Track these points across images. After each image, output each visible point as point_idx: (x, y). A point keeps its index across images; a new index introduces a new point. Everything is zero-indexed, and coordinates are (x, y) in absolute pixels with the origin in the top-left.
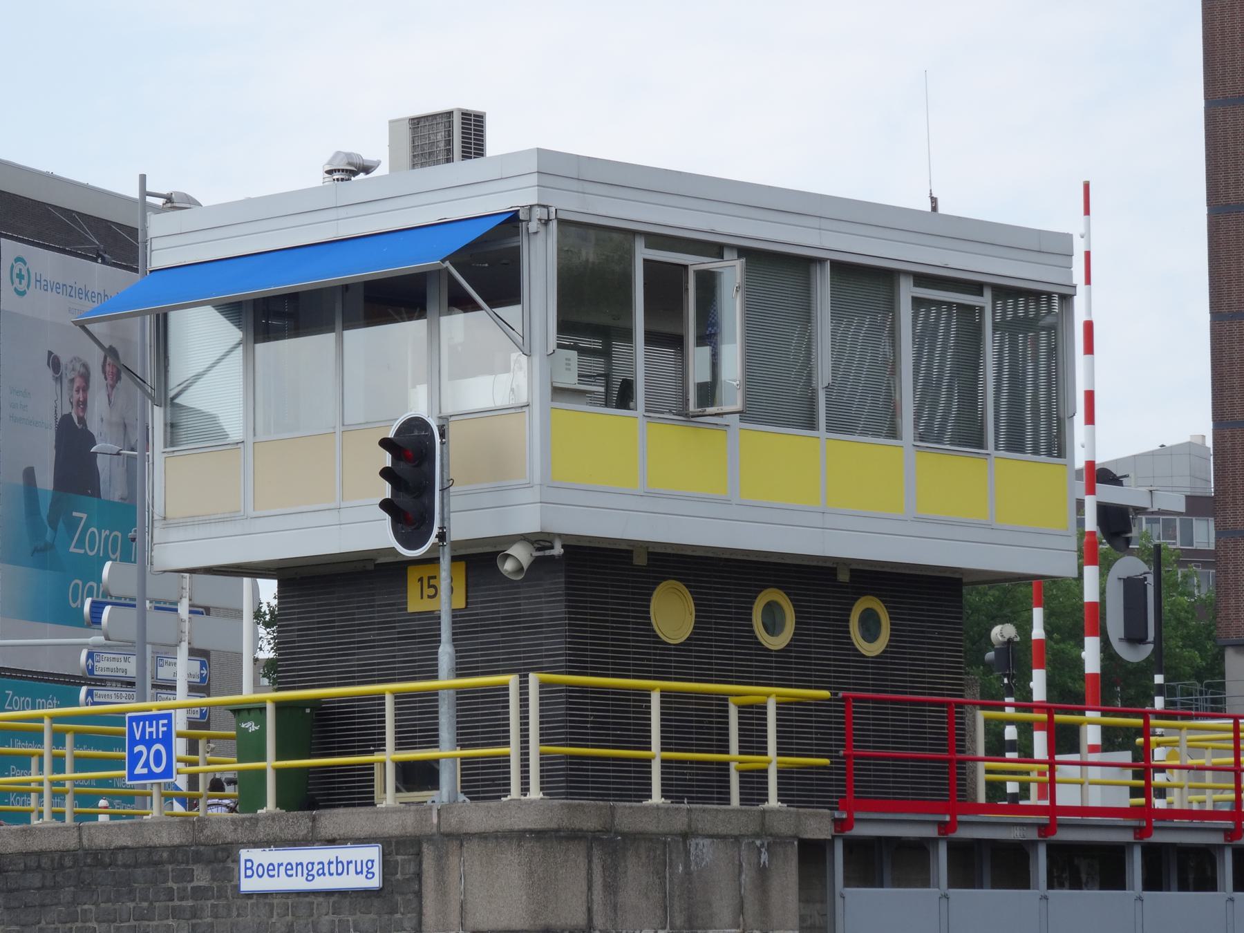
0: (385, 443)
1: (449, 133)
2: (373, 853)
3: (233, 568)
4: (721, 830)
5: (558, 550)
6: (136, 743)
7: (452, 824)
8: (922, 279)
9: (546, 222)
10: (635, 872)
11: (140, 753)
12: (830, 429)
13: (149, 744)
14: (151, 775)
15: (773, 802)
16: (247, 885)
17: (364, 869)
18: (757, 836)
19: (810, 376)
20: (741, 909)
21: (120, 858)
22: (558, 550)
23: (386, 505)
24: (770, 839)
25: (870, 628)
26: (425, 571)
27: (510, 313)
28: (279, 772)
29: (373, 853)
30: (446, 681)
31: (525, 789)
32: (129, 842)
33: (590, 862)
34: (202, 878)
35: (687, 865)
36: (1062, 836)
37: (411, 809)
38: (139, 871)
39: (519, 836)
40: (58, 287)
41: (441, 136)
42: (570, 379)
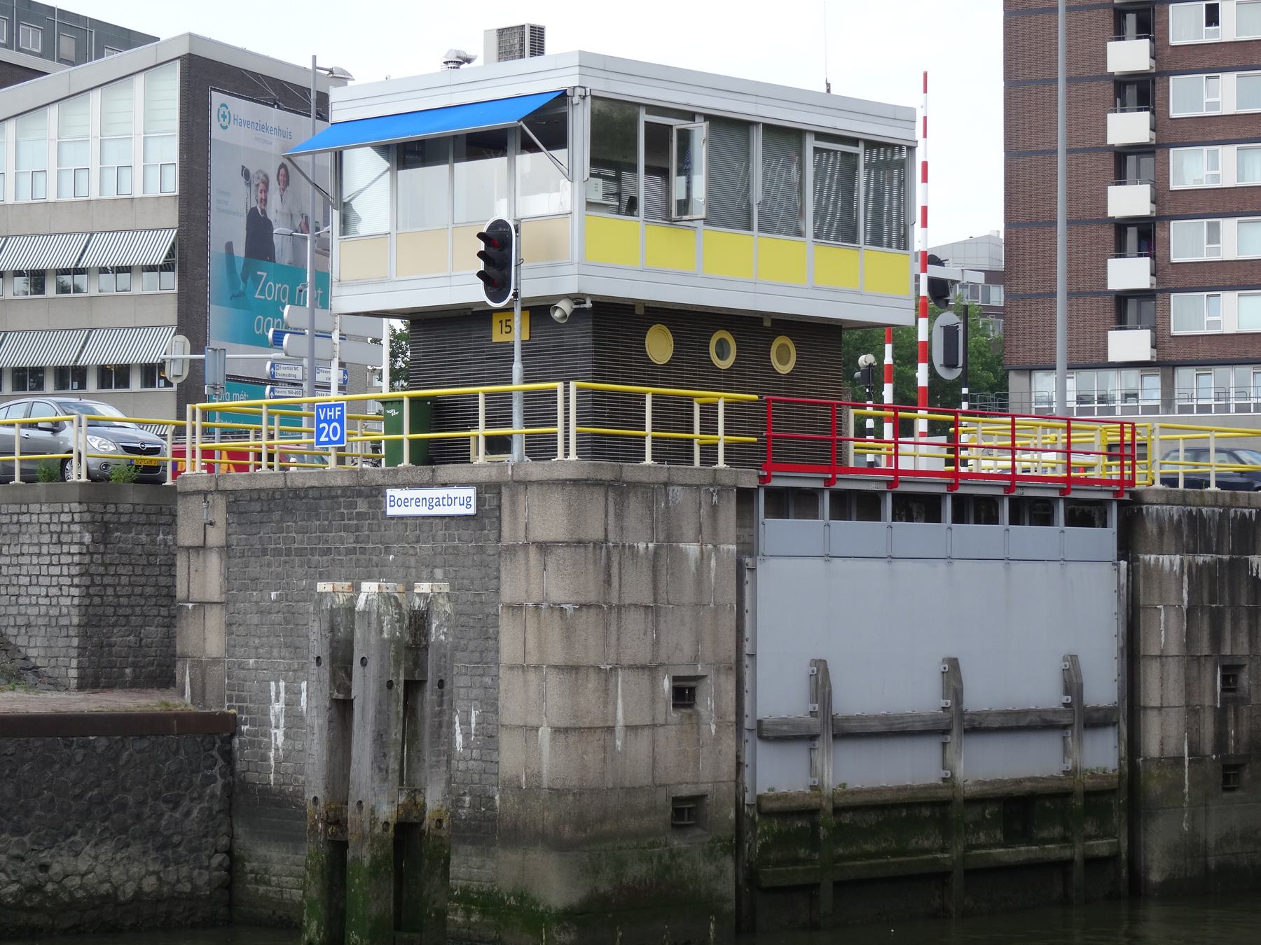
0: (481, 236)
1: (522, 39)
2: (471, 492)
4: (689, 481)
5: (589, 305)
7: (521, 474)
8: (820, 136)
9: (584, 97)
10: (635, 506)
11: (324, 428)
13: (329, 422)
14: (331, 442)
15: (721, 464)
16: (391, 511)
18: (711, 485)
19: (748, 190)
22: (589, 305)
23: (481, 275)
24: (719, 487)
27: (560, 154)
28: (412, 441)
29: (471, 492)
30: (517, 385)
31: (567, 454)
33: (607, 500)
34: (362, 506)
35: (667, 503)
36: (902, 488)
39: (562, 483)
40: (248, 124)
41: (517, 41)
42: (598, 197)
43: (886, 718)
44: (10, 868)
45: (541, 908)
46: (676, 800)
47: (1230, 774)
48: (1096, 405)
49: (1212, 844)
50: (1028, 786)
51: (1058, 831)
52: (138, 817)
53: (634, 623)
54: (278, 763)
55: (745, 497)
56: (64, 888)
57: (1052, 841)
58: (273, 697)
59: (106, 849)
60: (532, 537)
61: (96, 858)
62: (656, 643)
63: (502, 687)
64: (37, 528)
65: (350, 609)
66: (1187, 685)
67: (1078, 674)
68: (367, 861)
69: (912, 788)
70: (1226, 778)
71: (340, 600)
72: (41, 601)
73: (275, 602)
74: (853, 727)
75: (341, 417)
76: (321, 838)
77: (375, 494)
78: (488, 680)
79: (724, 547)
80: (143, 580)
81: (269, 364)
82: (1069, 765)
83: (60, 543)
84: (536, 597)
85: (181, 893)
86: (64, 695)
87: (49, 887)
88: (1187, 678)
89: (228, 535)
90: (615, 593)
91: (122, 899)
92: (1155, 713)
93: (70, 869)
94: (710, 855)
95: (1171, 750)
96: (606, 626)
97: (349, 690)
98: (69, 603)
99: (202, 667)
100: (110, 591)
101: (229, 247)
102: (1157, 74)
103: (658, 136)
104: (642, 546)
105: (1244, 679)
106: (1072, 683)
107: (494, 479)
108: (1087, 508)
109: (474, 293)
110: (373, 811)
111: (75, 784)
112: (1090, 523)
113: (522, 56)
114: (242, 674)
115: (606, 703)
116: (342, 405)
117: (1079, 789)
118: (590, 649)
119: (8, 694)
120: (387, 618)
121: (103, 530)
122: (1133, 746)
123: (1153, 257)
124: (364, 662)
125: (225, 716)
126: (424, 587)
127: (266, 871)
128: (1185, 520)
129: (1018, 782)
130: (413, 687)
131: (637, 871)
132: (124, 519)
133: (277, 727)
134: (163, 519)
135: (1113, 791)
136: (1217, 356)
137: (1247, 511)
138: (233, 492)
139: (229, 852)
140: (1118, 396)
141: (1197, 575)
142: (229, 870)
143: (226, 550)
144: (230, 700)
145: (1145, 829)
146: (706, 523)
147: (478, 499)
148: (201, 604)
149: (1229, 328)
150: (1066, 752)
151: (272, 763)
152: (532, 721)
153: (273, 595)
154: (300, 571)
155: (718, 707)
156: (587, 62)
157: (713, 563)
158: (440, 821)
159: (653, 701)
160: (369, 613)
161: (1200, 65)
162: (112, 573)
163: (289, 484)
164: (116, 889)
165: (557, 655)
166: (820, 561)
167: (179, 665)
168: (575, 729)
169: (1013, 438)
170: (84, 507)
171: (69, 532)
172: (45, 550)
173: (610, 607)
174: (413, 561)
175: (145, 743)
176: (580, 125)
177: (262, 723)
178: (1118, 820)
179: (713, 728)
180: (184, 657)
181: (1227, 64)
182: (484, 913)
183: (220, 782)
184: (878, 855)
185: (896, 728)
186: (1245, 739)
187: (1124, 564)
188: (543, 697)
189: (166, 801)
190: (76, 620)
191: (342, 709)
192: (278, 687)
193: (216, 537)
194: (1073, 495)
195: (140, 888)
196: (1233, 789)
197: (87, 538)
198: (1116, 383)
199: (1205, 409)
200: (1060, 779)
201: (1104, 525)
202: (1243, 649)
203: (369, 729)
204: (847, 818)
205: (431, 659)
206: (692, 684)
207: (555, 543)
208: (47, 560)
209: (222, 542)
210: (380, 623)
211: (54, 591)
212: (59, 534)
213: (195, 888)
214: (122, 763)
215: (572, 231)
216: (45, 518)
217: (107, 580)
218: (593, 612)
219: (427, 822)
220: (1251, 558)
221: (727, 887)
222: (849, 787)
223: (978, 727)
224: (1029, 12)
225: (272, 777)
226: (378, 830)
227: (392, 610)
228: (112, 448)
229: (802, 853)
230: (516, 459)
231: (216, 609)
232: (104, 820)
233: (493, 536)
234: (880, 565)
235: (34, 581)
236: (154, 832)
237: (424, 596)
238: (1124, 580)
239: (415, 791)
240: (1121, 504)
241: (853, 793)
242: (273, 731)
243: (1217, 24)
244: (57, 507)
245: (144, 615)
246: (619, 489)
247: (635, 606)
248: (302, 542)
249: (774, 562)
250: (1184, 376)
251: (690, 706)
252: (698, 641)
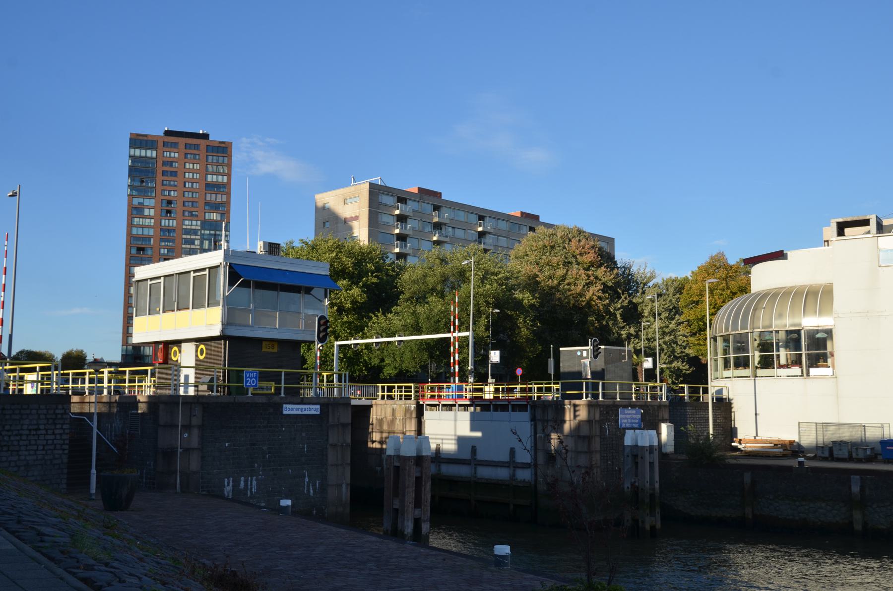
2: (318, 406)
3: (776, 456)
6: (248, 378)
11: (248, 380)
16: (285, 412)
29: (318, 406)
37: (9, 427)
58: (226, 484)
73: (227, 447)
77: (279, 407)
116: (257, 372)
153: (227, 445)
163: (236, 401)
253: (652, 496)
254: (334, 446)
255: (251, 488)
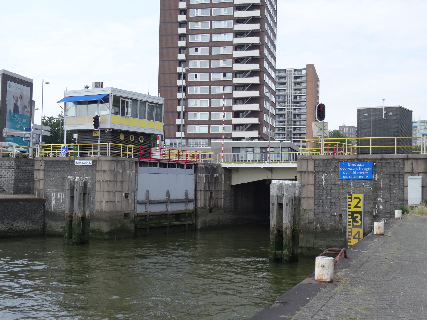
0: (94, 118)
1: (99, 84)
2: (91, 161)
4: (128, 160)
5: (112, 130)
7: (100, 159)
8: (149, 102)
9: (112, 95)
10: (119, 164)
12: (139, 118)
13: (64, 149)
14: (64, 152)
15: (133, 157)
16: (76, 164)
17: (90, 163)
19: (137, 112)
20: (129, 169)
21: (61, 161)
22: (112, 130)
23: (93, 125)
25: (141, 139)
26: (98, 131)
27: (107, 104)
28: (80, 152)
29: (91, 161)
30: (99, 143)
31: (108, 155)
32: (62, 159)
34: (70, 163)
36: (161, 162)
38: (63, 162)
39: (108, 160)
40: (14, 87)
41: (98, 84)
42: (113, 112)
43: (158, 200)
44: (6, 225)
45: (102, 232)
46: (125, 213)
47: (211, 210)
48: (174, 145)
49: (208, 221)
50: (179, 212)
51: (184, 219)
52: (28, 216)
53: (119, 184)
54: (53, 207)
55: (136, 163)
56: (15, 229)
57: (183, 221)
59: (23, 222)
60: (102, 169)
61: (21, 224)
62: (122, 187)
63: (96, 194)
64: (5, 166)
65: (74, 181)
66: (204, 195)
67: (188, 193)
68: (77, 223)
69: (161, 212)
70: (210, 211)
71: (72, 179)
72: (6, 178)
74: (153, 202)
75: (66, 148)
76: (68, 220)
77: (73, 161)
78: (93, 193)
79: (133, 171)
80: (25, 175)
81: (24, 134)
82: (186, 208)
83: (10, 168)
84: (103, 179)
85: (36, 230)
86: (11, 195)
87: (13, 229)
88: (204, 194)
89: (44, 168)
90: (116, 179)
91: (25, 231)
92: (199, 200)
93: (17, 225)
94: (130, 223)
95: (202, 206)
96: (114, 184)
97: (74, 195)
98: (12, 179)
99: (39, 191)
100: (19, 177)
101: (10, 110)
102: (186, 86)
103: (123, 102)
104: (120, 171)
105: (213, 194)
106: (187, 195)
107: (95, 159)
108: (189, 166)
109: (92, 127)
110: (78, 215)
111: (18, 211)
112: (189, 168)
113: (99, 87)
114: (47, 192)
115: (114, 197)
117: (187, 212)
118: (112, 188)
119: (1, 195)
120: (81, 183)
121: (18, 166)
122: (196, 205)
123: (185, 119)
124: (77, 190)
125: (44, 199)
126: (86, 178)
127: (51, 226)
128: (205, 168)
129: (178, 211)
130: (85, 194)
131: (119, 225)
132: (22, 164)
133: (53, 201)
134: (28, 164)
135: (192, 213)
136: (195, 137)
137: (214, 166)
138: (46, 160)
139: (44, 223)
140: (178, 144)
141: (206, 177)
142: (44, 226)
143: (44, 170)
144: (44, 196)
145: (79, 241)
146: (130, 167)
147: (92, 162)
148: (39, 180)
149: (198, 132)
150: (185, 206)
151: (52, 207)
152: (101, 200)
153: (53, 178)
154: (58, 174)
155: (132, 198)
156: (113, 89)
157: (131, 174)
158: (88, 217)
159: (122, 197)
160: (78, 182)
161: (194, 85)
162: (337, 185)
164: (24, 229)
165: (106, 189)
166: (148, 174)
167: (35, 190)
168: (109, 202)
169: (170, 153)
170: (15, 162)
171: (12, 166)
172: (7, 169)
173: (115, 181)
174: (80, 173)
175: (30, 204)
176: (111, 99)
177: (51, 200)
178: (193, 218)
179: (131, 202)
180: (36, 189)
181: (198, 85)
182: (92, 232)
183: (43, 211)
184: (156, 223)
185: (159, 202)
186: (213, 204)
187: (195, 175)
188: (103, 196)
189: (33, 214)
190: (13, 182)
191: (72, 198)
192: (54, 194)
193: (42, 168)
194: (187, 163)
195: (28, 229)
196: (211, 213)
197: (15, 168)
198: (177, 141)
199: (193, 146)
200: (184, 211)
201: (192, 168)
202: (213, 189)
203: (77, 201)
204: (151, 217)
205: (87, 189)
206: (127, 194)
207: (106, 170)
208: (7, 171)
209: (43, 169)
210: (80, 183)
211: (8, 177)
212: (10, 167)
213: (38, 229)
214: (26, 207)
215: (109, 118)
216: (7, 164)
217: (18, 175)
218: (112, 182)
219: (86, 217)
220: (215, 174)
221: (132, 228)
222: (151, 212)
223: (172, 202)
224: (163, 73)
225: (52, 210)
226: (79, 218)
227: (82, 181)
228: (18, 152)
229: (144, 223)
230: (99, 156)
231: (42, 180)
232: (23, 217)
233: (95, 169)
234: (157, 174)
235: (5, 175)
236: (31, 219)
237: (86, 179)
238: (195, 178)
239: (84, 211)
240: (195, 165)
241: (152, 213)
242: (53, 202)
243: (197, 78)
244: (10, 162)
245: (25, 181)
246: (117, 161)
247: (119, 181)
248: (59, 169)
249: (141, 174)
250: (190, 140)
251: (127, 198)
252: (129, 187)
253: (280, 233)
254: (99, 181)
255: (62, 199)
